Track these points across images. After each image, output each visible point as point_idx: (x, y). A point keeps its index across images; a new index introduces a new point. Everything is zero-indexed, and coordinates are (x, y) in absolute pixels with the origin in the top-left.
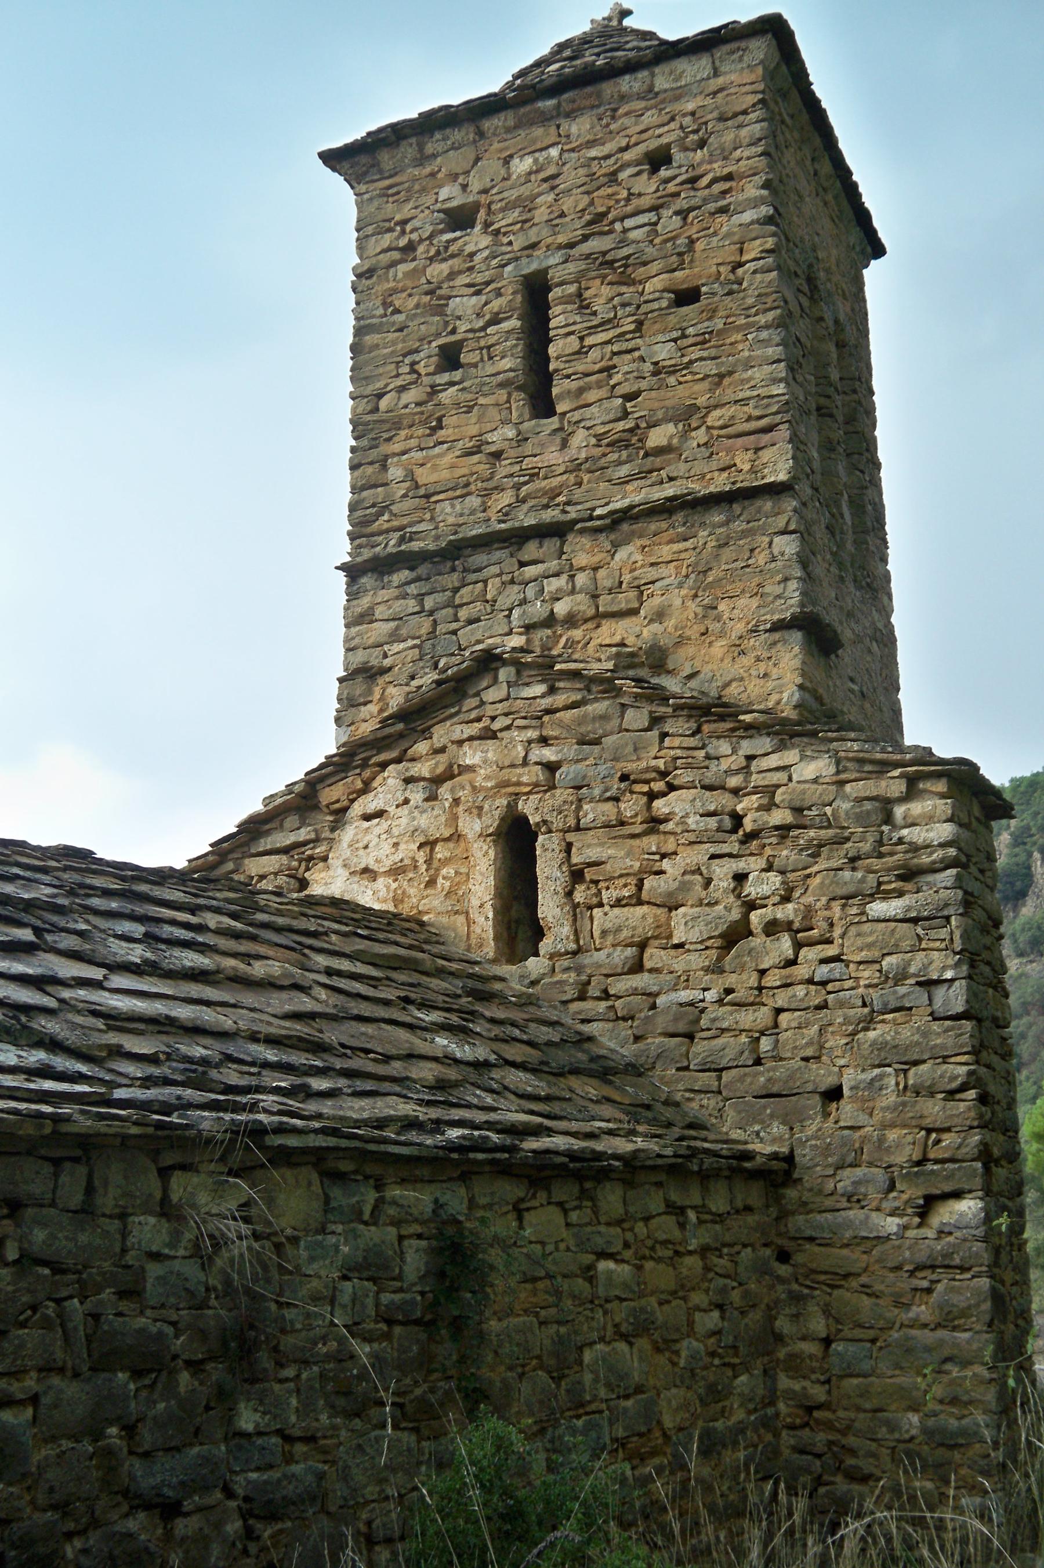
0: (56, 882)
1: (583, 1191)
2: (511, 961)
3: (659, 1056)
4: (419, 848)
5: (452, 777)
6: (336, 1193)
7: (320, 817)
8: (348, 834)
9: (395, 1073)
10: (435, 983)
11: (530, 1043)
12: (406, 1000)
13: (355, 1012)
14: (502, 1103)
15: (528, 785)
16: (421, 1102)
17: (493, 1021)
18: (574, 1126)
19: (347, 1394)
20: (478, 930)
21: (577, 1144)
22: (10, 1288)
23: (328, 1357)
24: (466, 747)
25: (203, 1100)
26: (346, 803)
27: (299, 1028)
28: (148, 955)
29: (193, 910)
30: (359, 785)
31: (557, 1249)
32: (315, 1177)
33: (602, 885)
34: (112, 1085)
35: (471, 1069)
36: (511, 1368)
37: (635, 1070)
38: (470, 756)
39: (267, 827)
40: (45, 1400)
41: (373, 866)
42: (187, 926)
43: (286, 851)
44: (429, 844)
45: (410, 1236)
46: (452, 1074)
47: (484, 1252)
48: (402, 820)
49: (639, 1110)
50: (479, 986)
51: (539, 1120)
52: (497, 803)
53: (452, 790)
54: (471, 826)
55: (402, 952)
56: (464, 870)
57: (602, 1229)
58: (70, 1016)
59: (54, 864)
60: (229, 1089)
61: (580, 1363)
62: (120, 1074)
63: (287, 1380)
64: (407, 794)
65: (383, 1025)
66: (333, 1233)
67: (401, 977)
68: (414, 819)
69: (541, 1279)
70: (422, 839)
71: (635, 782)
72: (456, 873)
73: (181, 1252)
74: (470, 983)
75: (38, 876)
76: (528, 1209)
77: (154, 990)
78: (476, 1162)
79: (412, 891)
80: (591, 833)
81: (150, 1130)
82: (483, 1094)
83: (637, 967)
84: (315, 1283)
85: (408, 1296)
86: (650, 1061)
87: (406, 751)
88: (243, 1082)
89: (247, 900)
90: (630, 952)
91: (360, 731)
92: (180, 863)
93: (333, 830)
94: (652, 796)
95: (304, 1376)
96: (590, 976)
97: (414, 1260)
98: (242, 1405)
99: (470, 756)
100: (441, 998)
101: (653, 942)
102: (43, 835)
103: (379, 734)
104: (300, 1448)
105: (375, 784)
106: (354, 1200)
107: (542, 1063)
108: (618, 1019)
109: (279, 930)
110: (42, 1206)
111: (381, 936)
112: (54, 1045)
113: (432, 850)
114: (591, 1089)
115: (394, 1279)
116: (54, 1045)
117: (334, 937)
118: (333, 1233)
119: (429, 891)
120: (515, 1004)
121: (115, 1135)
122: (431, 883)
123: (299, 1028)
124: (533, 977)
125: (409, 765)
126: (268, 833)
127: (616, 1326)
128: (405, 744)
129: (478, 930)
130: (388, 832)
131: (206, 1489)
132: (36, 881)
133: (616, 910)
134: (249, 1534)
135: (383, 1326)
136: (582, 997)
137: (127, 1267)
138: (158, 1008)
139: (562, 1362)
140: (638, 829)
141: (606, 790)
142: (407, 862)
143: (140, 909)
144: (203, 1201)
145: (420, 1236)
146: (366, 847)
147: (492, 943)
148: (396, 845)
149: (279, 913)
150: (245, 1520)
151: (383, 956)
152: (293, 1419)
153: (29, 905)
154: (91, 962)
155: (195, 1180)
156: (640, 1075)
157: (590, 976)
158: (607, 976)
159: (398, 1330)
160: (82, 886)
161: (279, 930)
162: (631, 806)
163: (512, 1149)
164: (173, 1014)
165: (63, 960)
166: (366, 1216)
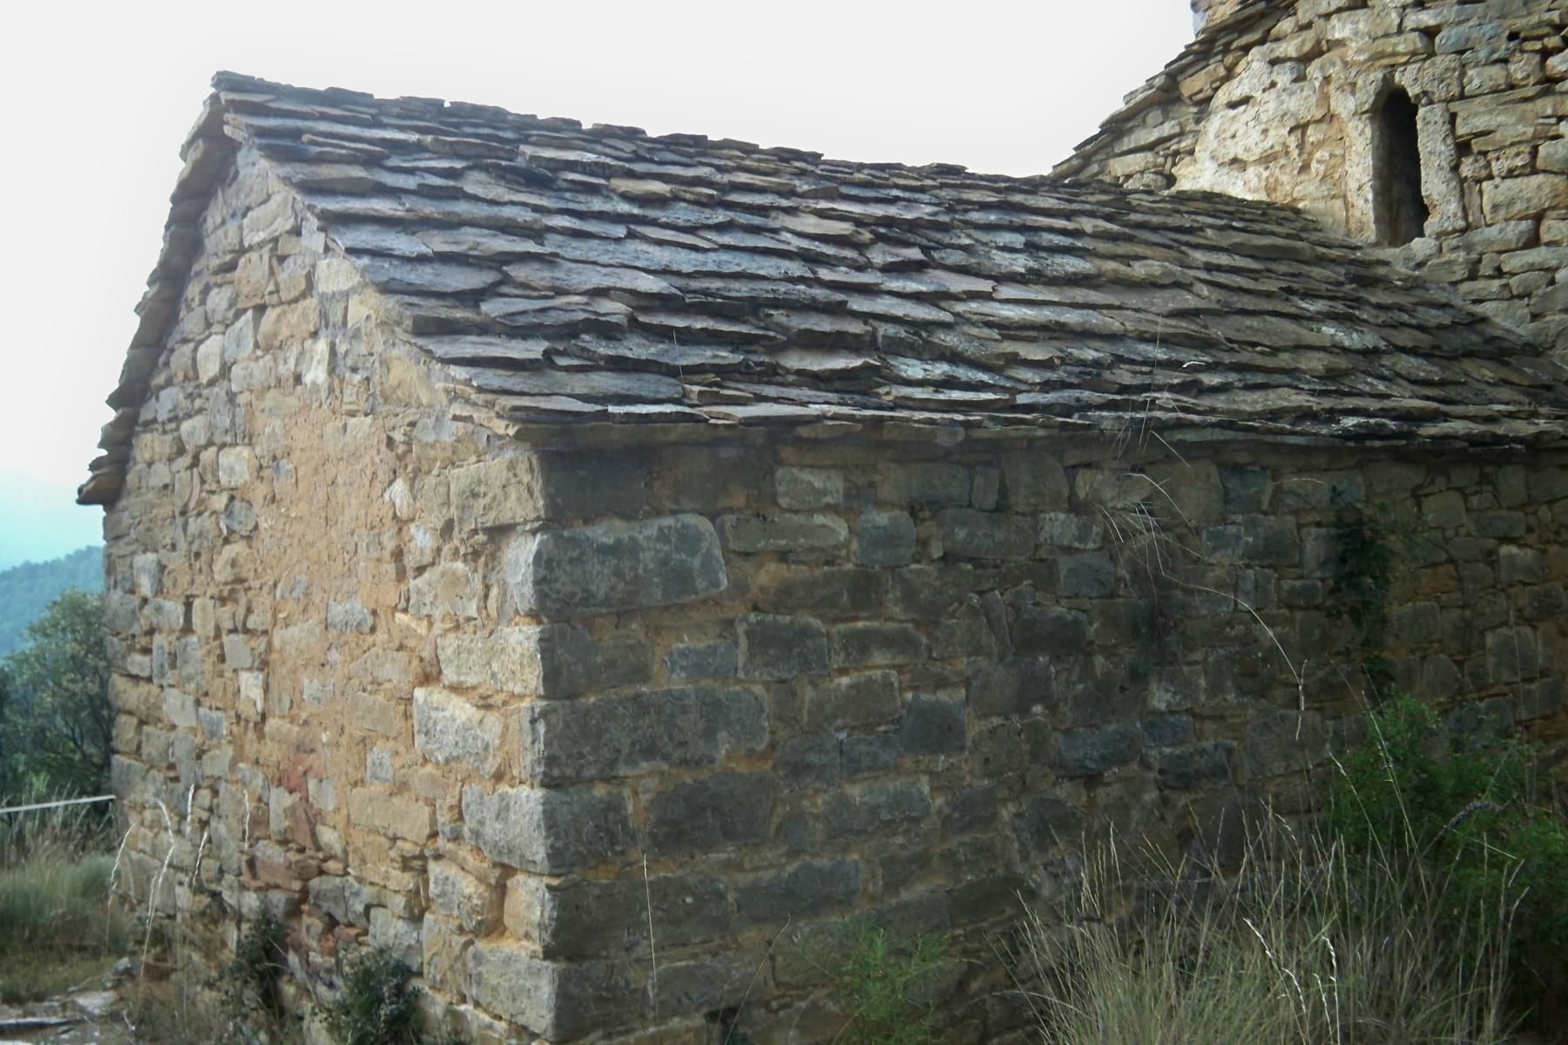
0: (934, 200)
1: (1483, 475)
2: (1394, 242)
3: (1559, 335)
4: (1291, 131)
5: (1321, 54)
6: (1233, 483)
7: (1184, 109)
8: (1213, 125)
9: (1283, 365)
10: (1316, 271)
11: (1421, 328)
12: (1290, 291)
13: (1239, 306)
14: (1395, 390)
15: (1404, 54)
16: (1313, 392)
17: (1380, 307)
18: (1472, 410)
19: (1254, 675)
20: (1357, 214)
21: (1477, 428)
22: (938, 583)
23: (1237, 639)
24: (1334, 20)
25: (1100, 401)
26: (1209, 92)
27: (1184, 326)
28: (1031, 264)
29: (1068, 215)
30: (1222, 72)
31: (1457, 534)
32: (1213, 470)
33: (1491, 156)
34: (1014, 392)
35: (1360, 358)
36: (1412, 652)
37: (1533, 350)
38: (1339, 29)
39: (1130, 125)
40: (976, 683)
41: (1242, 155)
42: (1064, 232)
43: (1150, 147)
44: (1300, 128)
45: (1307, 525)
46: (1343, 363)
47: (1383, 538)
48: (1269, 105)
49: (1539, 391)
50: (1362, 271)
51: (1435, 405)
52: (1372, 77)
53: (1322, 68)
54: (1344, 105)
55: (1280, 241)
56: (1338, 152)
57: (1504, 513)
58: (966, 328)
59: (929, 182)
60: (1123, 389)
61: (1482, 646)
62: (1020, 381)
63: (1196, 662)
64: (1274, 77)
65: (1267, 318)
66: (1234, 523)
67: (1282, 268)
68: (1282, 103)
69: (1440, 564)
70: (1292, 123)
71: (1525, 39)
72: (1331, 155)
73: (1091, 545)
74: (1353, 269)
75: (917, 196)
76: (1426, 496)
77: (1041, 297)
78: (1373, 449)
79: (1285, 178)
80: (1478, 100)
81: (1056, 431)
82: (1375, 382)
83: (1533, 241)
84: (1218, 571)
85: (1309, 582)
86: (1550, 339)
87: (1269, 31)
88: (1137, 381)
89: (1119, 200)
90: (1525, 225)
91: (1218, 15)
92: (1047, 171)
93: (1198, 121)
94: (1546, 53)
95: (1211, 659)
96: (1481, 254)
97: (1314, 546)
98: (1154, 686)
99: (1339, 29)
100: (1324, 287)
101: (1549, 213)
102: (917, 157)
103: (1240, 16)
104: (1209, 726)
105: (1239, 69)
106: (1253, 490)
107: (1434, 347)
108: (1513, 297)
109: (1155, 229)
110: (961, 506)
111: (1257, 227)
112: (954, 357)
113: (1304, 134)
114: (1487, 372)
115: (1295, 566)
116: (954, 357)
117: (1209, 232)
118: (1234, 523)
119: (1303, 177)
120: (1401, 288)
121: (1022, 438)
122: (1305, 168)
123: (1184, 326)
124: (1420, 258)
125: (1274, 45)
126: (1131, 131)
127: (1519, 610)
128: (1267, 24)
129: (1357, 214)
130: (1256, 118)
131: (1124, 762)
132: (916, 201)
133: (1508, 182)
134: (1165, 802)
135: (1285, 611)
136: (1473, 276)
137: (1042, 560)
138: (1047, 315)
139: (1467, 641)
140: (1530, 91)
141: (1493, 52)
142: (1278, 148)
143: (1018, 219)
144: (1109, 496)
145: (1318, 525)
146: (1234, 136)
147: (1373, 227)
148: (1265, 131)
149: (1153, 211)
150: (1161, 790)
151: (1257, 247)
152: (1203, 698)
153: (914, 225)
154: (978, 275)
155: (1100, 477)
156: (1538, 354)
157: (1481, 254)
158: (1500, 252)
159: (1299, 615)
160: (960, 201)
161: (1155, 229)
162: (1521, 68)
163: (1409, 435)
164: (1062, 319)
165: (952, 275)
166: (1265, 506)
